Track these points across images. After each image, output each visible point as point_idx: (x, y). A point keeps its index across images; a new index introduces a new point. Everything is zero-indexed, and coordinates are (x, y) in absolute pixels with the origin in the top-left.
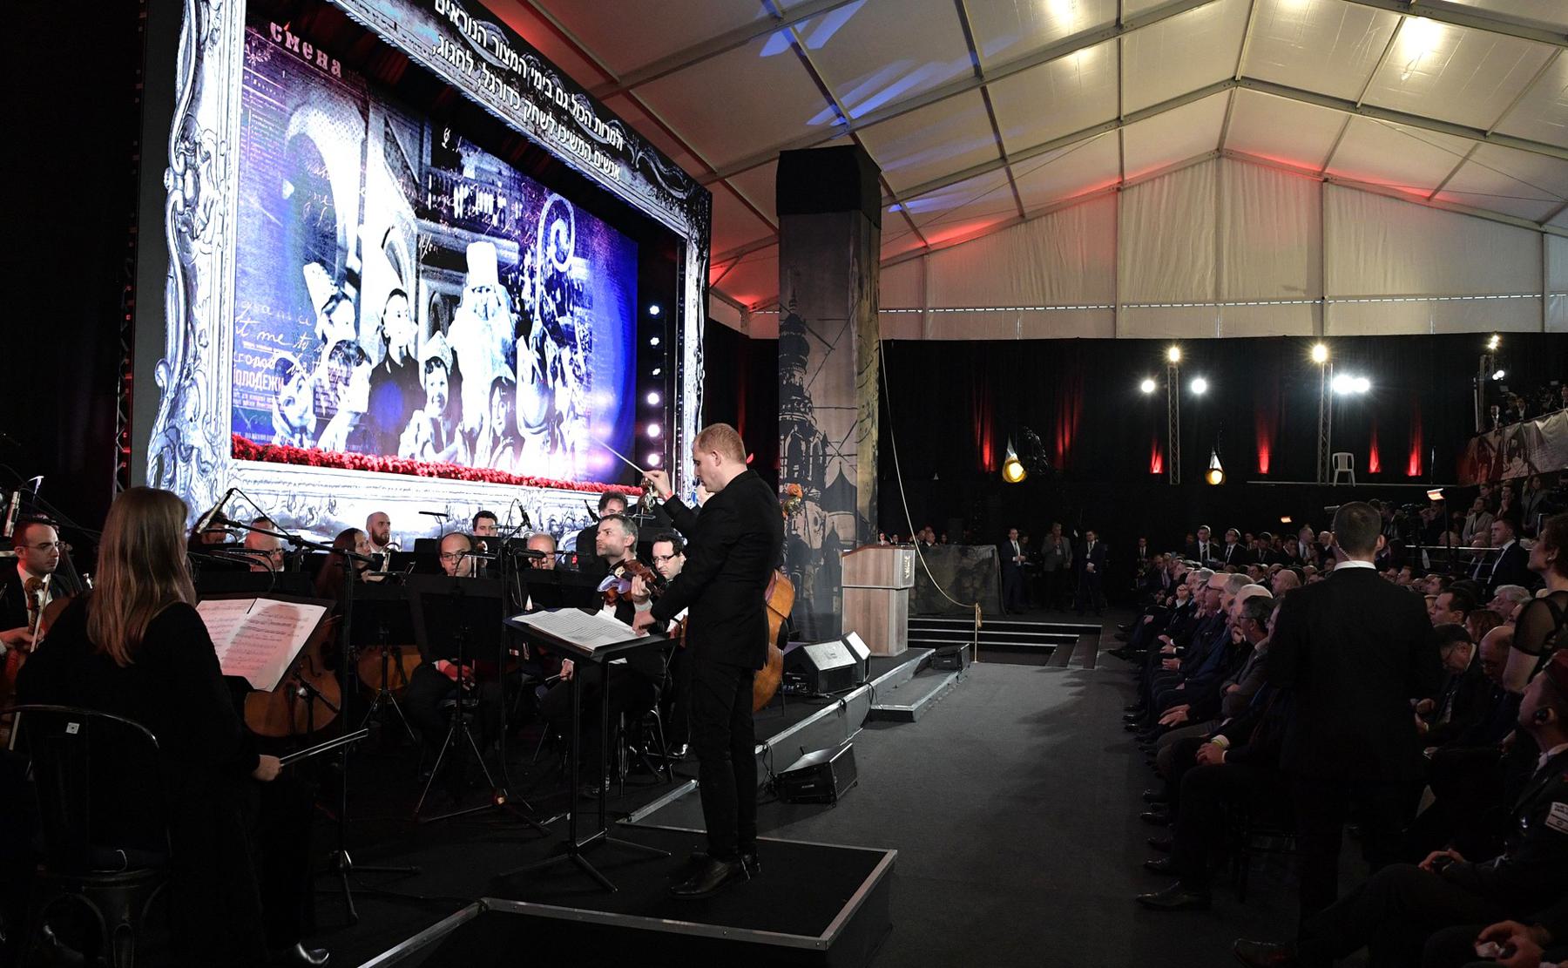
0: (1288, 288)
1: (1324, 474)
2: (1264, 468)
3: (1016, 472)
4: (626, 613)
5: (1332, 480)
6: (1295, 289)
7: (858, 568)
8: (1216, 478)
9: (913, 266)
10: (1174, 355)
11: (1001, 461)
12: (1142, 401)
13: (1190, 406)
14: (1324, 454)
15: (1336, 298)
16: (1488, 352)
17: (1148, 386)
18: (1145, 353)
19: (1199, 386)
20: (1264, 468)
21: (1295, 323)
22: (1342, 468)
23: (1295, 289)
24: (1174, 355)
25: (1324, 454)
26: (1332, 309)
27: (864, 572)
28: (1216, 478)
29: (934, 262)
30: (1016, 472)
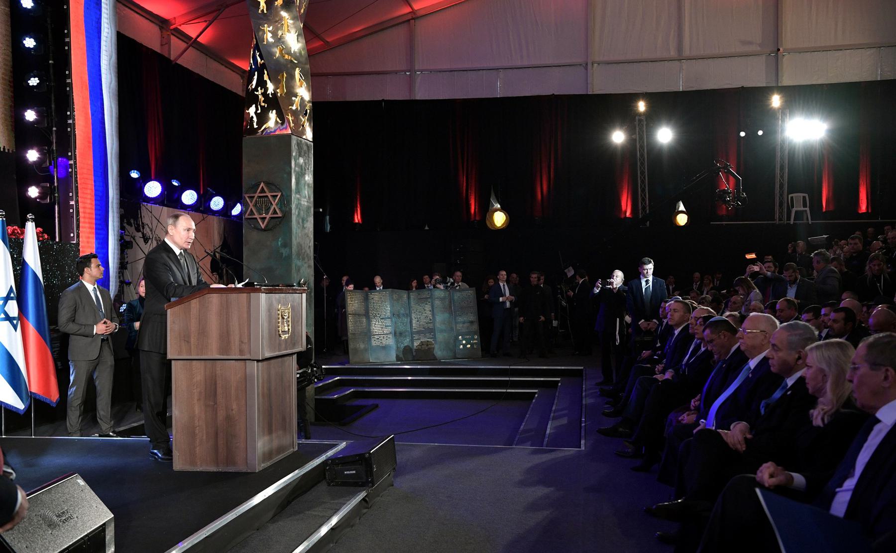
0: (744, 43)
1: (781, 213)
2: (863, 208)
3: (499, 219)
4: (887, 370)
5: (789, 218)
6: (750, 43)
7: (194, 326)
8: (682, 220)
9: (402, 31)
10: (642, 106)
11: (486, 211)
12: (610, 152)
13: (655, 154)
14: (781, 195)
15: (789, 51)
16: (640, 114)
17: (618, 137)
18: (616, 107)
19: (665, 135)
20: (863, 208)
21: (750, 74)
22: (798, 207)
23: (750, 43)
24: (642, 106)
25: (781, 195)
26: (787, 61)
27: (203, 333)
28: (682, 220)
29: (421, 27)
30: (499, 219)
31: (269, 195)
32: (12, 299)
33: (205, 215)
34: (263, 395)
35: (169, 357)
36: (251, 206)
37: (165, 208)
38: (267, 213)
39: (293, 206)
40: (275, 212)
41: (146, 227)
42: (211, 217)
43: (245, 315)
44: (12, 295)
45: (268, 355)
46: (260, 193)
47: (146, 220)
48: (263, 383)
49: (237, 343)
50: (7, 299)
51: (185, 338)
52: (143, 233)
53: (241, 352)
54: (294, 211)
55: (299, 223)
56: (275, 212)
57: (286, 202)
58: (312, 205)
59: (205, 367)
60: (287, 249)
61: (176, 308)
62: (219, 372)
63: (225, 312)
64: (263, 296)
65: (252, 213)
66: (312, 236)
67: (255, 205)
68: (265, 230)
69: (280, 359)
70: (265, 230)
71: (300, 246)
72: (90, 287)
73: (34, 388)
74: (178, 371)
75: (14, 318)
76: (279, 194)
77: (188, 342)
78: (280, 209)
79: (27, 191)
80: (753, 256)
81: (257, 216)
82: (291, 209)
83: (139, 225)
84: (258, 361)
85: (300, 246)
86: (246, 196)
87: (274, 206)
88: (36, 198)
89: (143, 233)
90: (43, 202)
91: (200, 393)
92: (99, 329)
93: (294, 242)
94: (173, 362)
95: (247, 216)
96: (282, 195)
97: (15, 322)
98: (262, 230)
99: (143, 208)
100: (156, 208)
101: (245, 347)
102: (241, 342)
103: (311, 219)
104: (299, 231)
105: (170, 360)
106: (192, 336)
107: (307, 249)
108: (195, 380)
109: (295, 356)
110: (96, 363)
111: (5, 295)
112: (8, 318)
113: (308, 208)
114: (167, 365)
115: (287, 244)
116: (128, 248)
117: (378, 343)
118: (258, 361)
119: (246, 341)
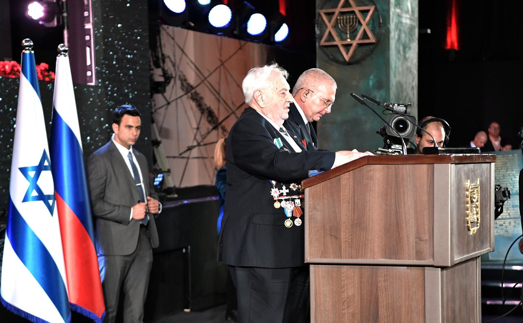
7: (345, 214)
27: (359, 223)
31: (356, 9)
32: (46, 168)
33: (243, 42)
34: (447, 319)
35: (308, 259)
36: (330, 27)
37: (191, 33)
38: (353, 38)
39: (392, 26)
40: (365, 36)
41: (167, 60)
42: (250, 44)
43: (425, 198)
44: (46, 163)
45: (457, 259)
46: (343, 6)
47: (167, 49)
48: (447, 299)
49: (412, 239)
50: (39, 169)
51: (332, 231)
52: (163, 70)
53: (419, 254)
54: (393, 35)
55: (398, 52)
56: (365, 36)
57: (381, 23)
58: (416, 24)
59: (361, 277)
60: (382, 92)
61: (319, 187)
62: (381, 284)
63: (393, 192)
64: (452, 168)
65: (330, 37)
66: (415, 72)
67: (335, 26)
68: (349, 64)
69: (464, 265)
70: (349, 64)
71: (400, 85)
72: (124, 152)
73: (73, 299)
74: (317, 278)
75: (49, 197)
76: (372, 9)
77: (336, 237)
78: (373, 31)
79: (26, 9)
80: (192, 24)
81: (338, 42)
82: (388, 31)
83: (157, 57)
84: (443, 268)
85: (400, 85)
86: (322, 12)
87: (364, 26)
88: (41, 19)
89: (163, 70)
90: (48, 25)
91: (353, 315)
92: (137, 212)
93: (394, 80)
94: (312, 267)
95: (323, 42)
96: (376, 9)
97: (51, 202)
98: (345, 63)
99: (161, 29)
100: (178, 31)
101: (425, 247)
102: (419, 239)
103: (415, 46)
104: (399, 64)
105: (308, 264)
106: (343, 229)
107: (409, 91)
108: (344, 296)
109: (479, 260)
110: (130, 261)
111: (37, 164)
112: (41, 197)
113: (412, 28)
114: (302, 271)
115: (383, 83)
116: (158, 92)
117: (502, 233)
118: (443, 268)
119: (426, 237)
